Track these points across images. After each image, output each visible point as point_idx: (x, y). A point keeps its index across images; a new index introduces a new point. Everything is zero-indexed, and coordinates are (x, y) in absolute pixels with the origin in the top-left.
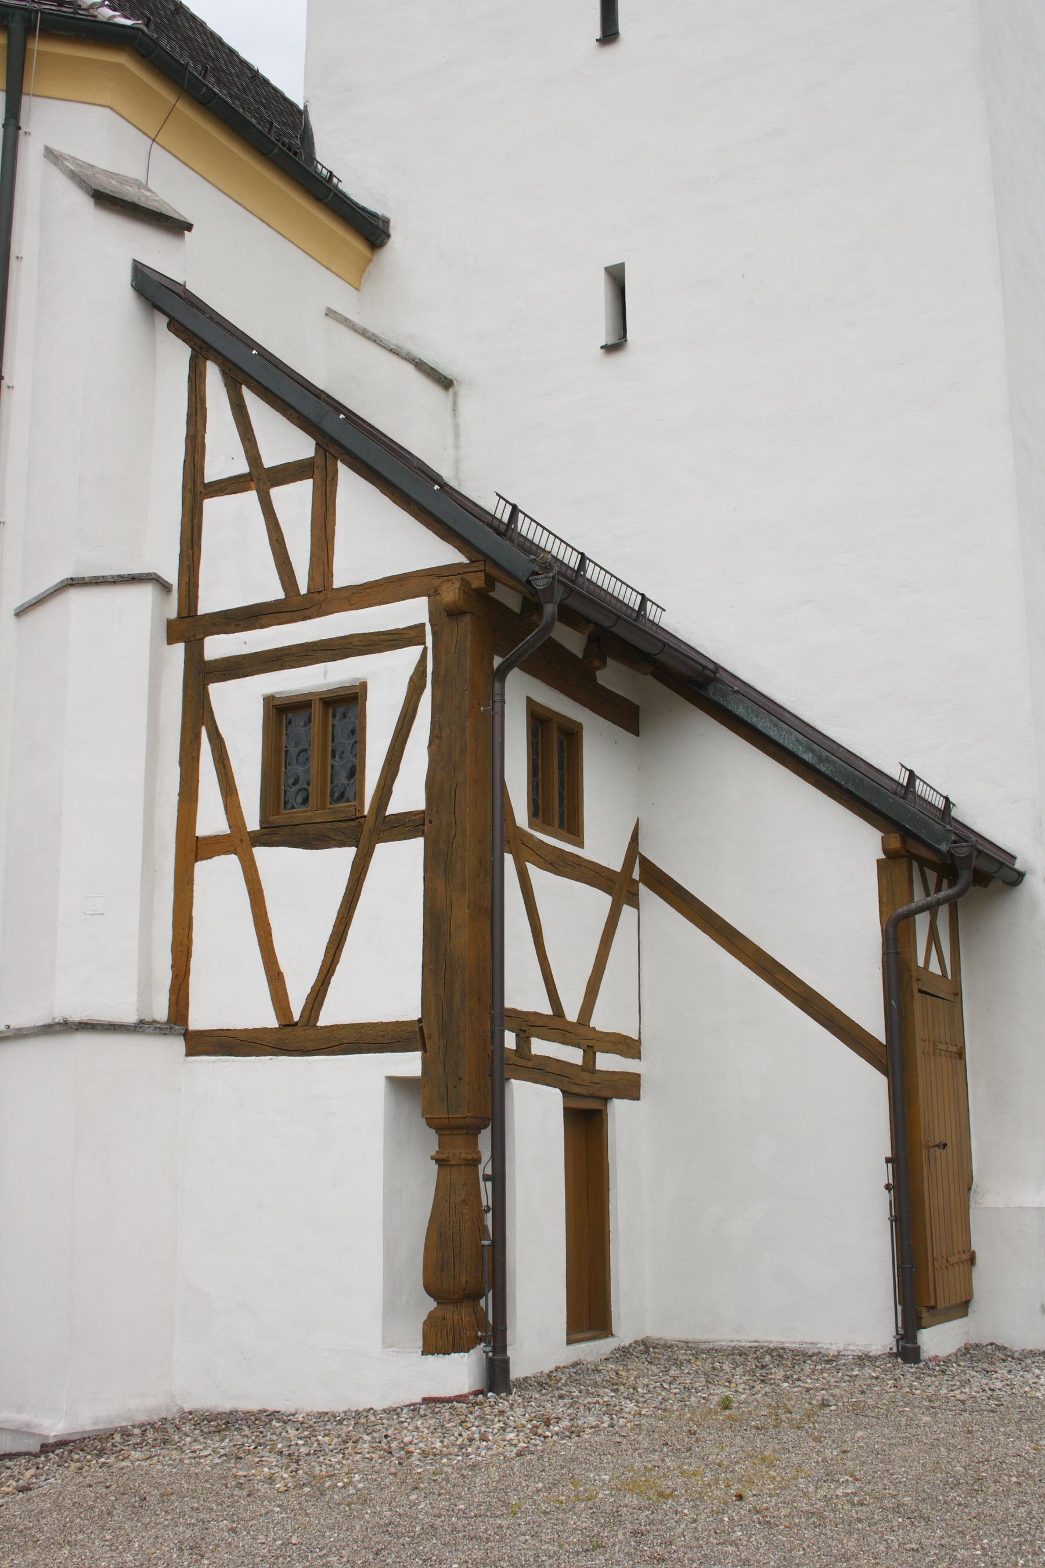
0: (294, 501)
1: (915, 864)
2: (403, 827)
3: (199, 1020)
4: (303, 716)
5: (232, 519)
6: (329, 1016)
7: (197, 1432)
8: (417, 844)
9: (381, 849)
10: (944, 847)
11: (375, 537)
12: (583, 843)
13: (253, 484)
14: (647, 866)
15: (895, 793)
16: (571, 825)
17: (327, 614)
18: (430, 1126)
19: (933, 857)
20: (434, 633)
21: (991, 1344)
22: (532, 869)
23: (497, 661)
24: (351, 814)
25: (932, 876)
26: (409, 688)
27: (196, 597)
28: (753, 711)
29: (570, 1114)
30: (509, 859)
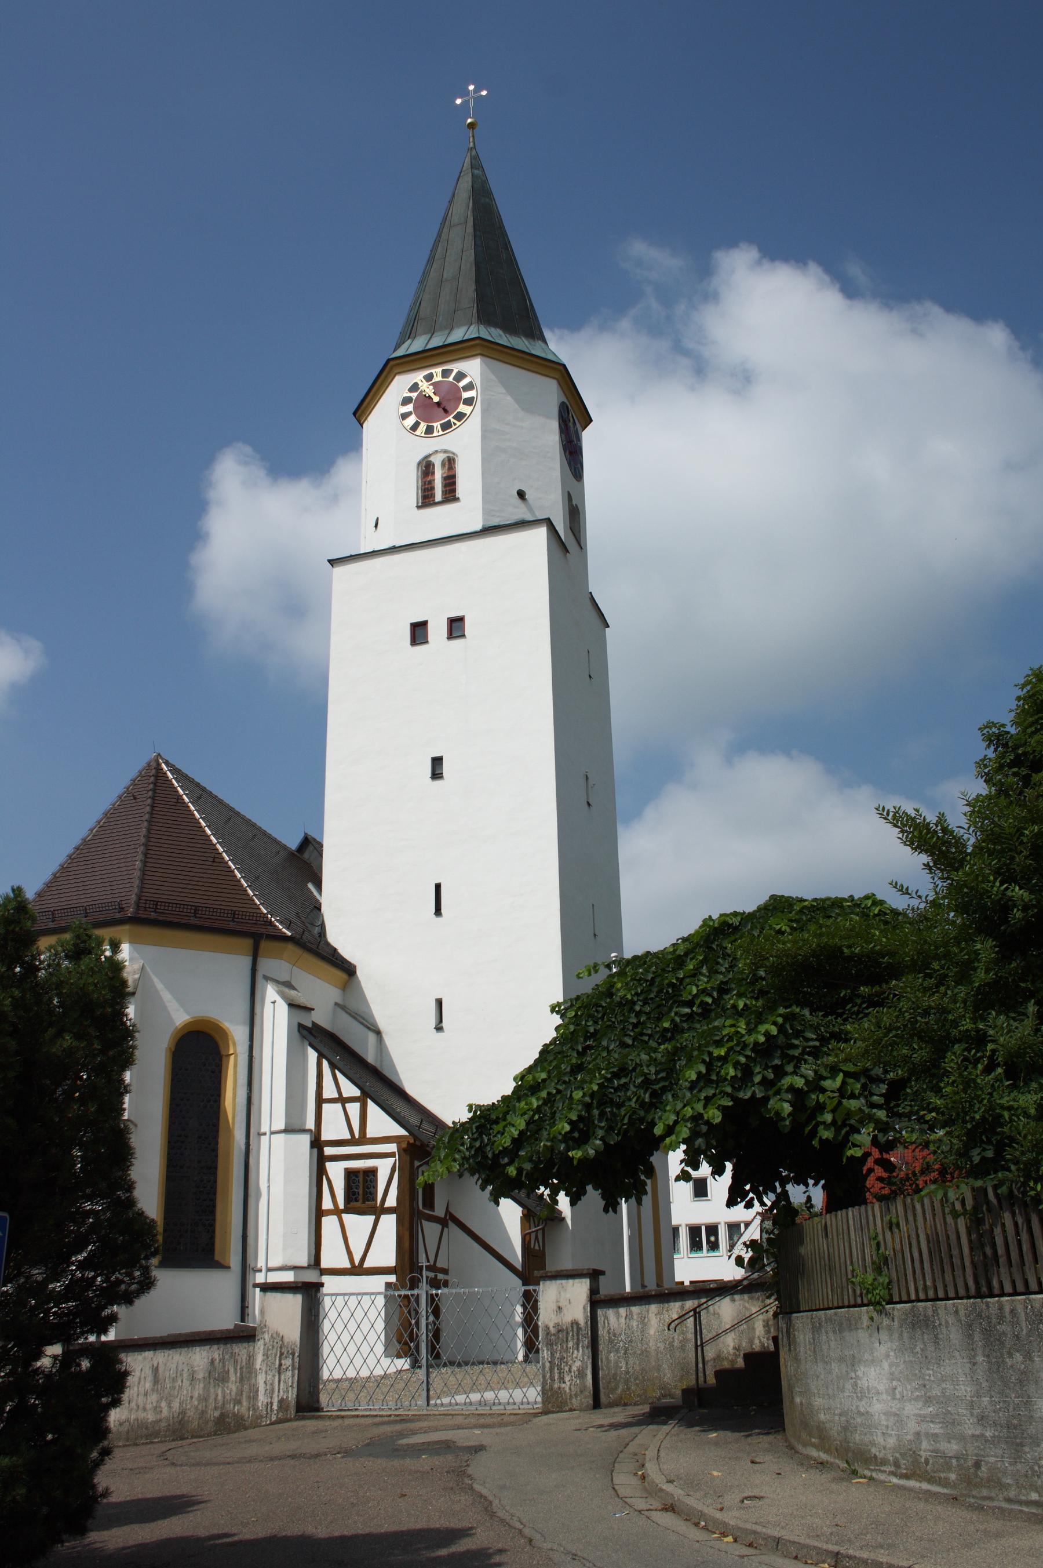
0: (354, 1109)
2: (390, 1211)
6: (366, 1265)
8: (394, 1216)
9: (382, 1216)
11: (381, 1123)
14: (451, 1214)
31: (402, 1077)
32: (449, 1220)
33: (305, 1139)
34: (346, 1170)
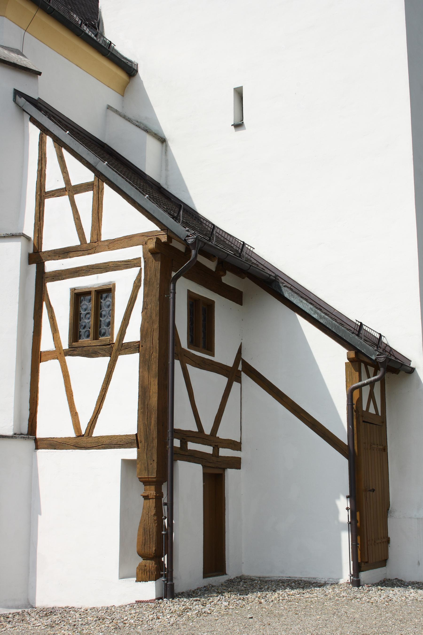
0: (85, 200)
1: (363, 365)
3: (40, 433)
4: (88, 297)
5: (57, 209)
6: (98, 431)
7: (37, 616)
8: (136, 357)
9: (120, 358)
10: (373, 358)
11: (123, 218)
12: (214, 354)
13: (67, 193)
15: (353, 333)
16: (209, 348)
17: (98, 252)
18: (141, 481)
19: (370, 362)
20: (145, 262)
21: (396, 579)
22: (189, 367)
23: (173, 274)
24: (108, 342)
25: (371, 370)
26: (134, 286)
27: (42, 243)
28: (292, 295)
29: (206, 476)
30: (177, 363)
31: (192, 192)
32: (239, 370)
33: (15, 250)
34: (73, 290)
